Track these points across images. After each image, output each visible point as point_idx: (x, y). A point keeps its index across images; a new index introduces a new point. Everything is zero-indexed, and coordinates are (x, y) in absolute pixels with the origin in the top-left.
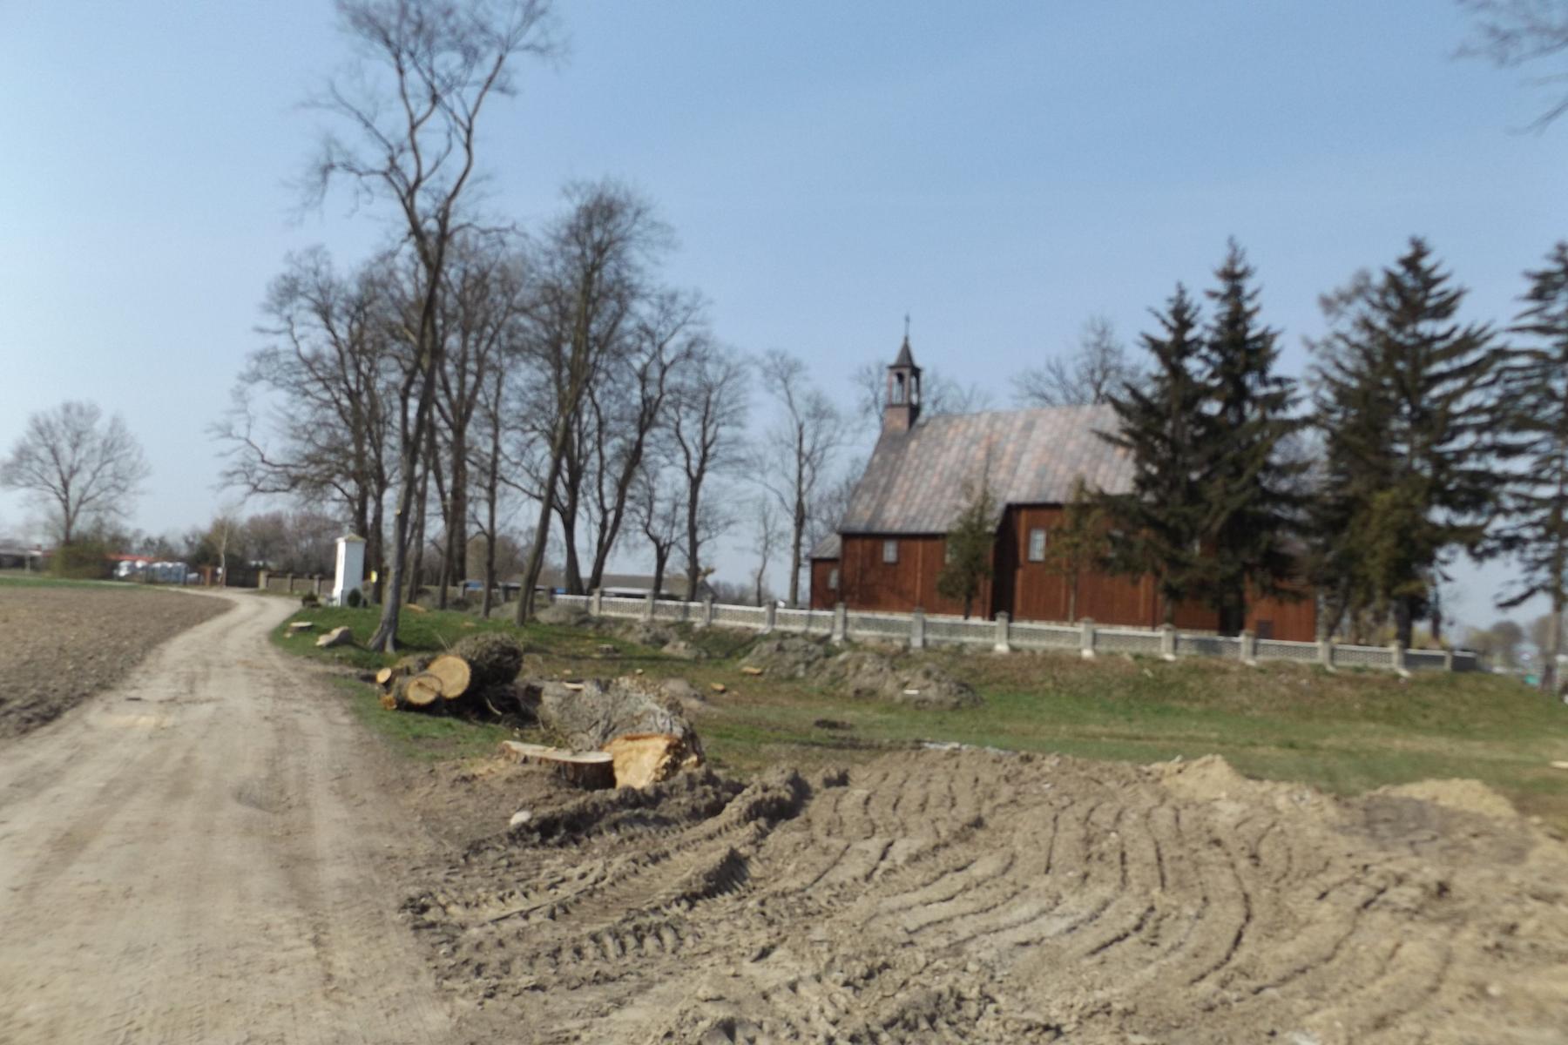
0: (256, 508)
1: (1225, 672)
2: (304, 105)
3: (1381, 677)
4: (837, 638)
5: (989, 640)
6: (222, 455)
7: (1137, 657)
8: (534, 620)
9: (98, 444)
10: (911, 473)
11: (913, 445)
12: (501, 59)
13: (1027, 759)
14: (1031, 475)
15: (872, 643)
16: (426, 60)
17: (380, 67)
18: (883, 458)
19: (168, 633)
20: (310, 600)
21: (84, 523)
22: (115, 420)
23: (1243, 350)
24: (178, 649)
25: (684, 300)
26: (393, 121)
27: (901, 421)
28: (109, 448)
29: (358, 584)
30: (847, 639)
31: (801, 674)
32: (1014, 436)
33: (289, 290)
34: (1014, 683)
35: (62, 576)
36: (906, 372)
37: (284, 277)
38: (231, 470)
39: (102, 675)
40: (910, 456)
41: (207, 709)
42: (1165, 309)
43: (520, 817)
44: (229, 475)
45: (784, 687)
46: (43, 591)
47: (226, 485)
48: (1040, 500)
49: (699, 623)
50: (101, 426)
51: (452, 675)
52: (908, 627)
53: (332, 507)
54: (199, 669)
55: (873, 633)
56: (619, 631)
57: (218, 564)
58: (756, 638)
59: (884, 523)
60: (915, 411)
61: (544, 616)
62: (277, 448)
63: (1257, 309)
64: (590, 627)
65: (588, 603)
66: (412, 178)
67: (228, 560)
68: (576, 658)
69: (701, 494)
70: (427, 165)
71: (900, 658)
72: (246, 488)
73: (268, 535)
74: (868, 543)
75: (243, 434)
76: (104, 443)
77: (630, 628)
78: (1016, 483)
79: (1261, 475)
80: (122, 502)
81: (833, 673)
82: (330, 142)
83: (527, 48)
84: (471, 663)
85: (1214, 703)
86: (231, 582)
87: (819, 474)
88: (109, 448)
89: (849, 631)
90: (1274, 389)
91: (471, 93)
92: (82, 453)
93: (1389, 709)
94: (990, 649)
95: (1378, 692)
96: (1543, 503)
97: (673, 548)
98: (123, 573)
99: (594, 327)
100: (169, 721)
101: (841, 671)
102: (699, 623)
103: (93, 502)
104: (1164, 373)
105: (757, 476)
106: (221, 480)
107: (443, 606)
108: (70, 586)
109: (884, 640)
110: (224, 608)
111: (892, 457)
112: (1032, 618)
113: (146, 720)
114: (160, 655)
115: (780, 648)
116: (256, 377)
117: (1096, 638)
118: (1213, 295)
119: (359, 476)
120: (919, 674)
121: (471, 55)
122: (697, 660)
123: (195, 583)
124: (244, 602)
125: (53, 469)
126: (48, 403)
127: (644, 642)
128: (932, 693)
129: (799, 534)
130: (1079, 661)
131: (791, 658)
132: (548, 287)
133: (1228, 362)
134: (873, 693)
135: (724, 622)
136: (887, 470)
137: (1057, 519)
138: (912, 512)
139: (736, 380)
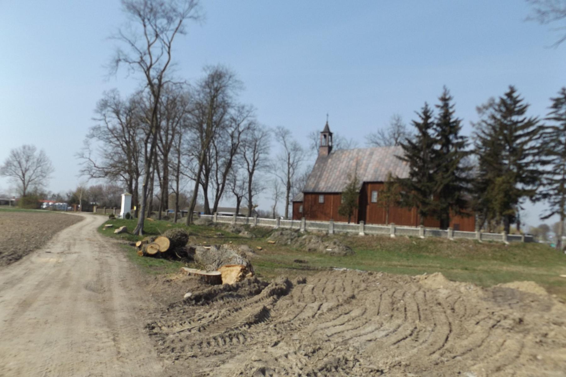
0: (92, 183)
1: (442, 242)
2: (110, 38)
3: (499, 244)
4: (302, 230)
5: (357, 231)
6: (80, 164)
7: (410, 237)
8: (193, 224)
9: (35, 160)
10: (329, 171)
11: (330, 160)
12: (181, 21)
14: (372, 172)
15: (315, 232)
16: (154, 22)
17: (137, 24)
18: (319, 165)
19: (60, 228)
20: (112, 216)
21: (30, 189)
22: (41, 152)
23: (449, 126)
24: (64, 234)
25: (247, 108)
26: (142, 44)
27: (325, 152)
28: (39, 162)
29: (129, 211)
30: (306, 230)
31: (289, 243)
32: (366, 157)
33: (104, 105)
34: (366, 246)
35: (23, 208)
36: (327, 134)
37: (103, 100)
38: (83, 169)
39: (37, 243)
40: (328, 164)
41: (75, 256)
42: (420, 111)
43: (188, 295)
44: (83, 171)
45: (283, 248)
46: (15, 213)
47: (81, 175)
48: (375, 180)
49: (252, 225)
50: (36, 154)
51: (163, 243)
52: (328, 226)
53: (120, 183)
54: (72, 241)
55: (315, 228)
56: (224, 228)
57: (79, 204)
58: (273, 230)
59: (319, 189)
60: (330, 148)
61: (196, 222)
62: (100, 161)
63: (454, 112)
64: (213, 226)
65: (212, 218)
66: (149, 64)
67: (82, 202)
68: (208, 237)
69: (253, 178)
70: (154, 59)
71: (325, 237)
72: (89, 176)
74: (313, 196)
75: (88, 156)
76: (38, 160)
77: (227, 227)
78: (367, 174)
79: (455, 171)
80: (44, 181)
81: (301, 243)
82: (119, 51)
83: (190, 17)
84: (170, 239)
85: (438, 254)
86: (83, 210)
87: (296, 171)
88: (39, 162)
89: (307, 228)
90: (460, 140)
91: (170, 34)
92: (30, 163)
93: (501, 256)
94: (357, 234)
95: (497, 250)
96: (557, 181)
97: (243, 198)
98: (44, 207)
100: (61, 260)
101: (304, 242)
102: (252, 225)
104: (420, 134)
105: (273, 172)
106: (80, 173)
107: (160, 219)
108: (25, 211)
109: (319, 231)
110: (81, 219)
111: (322, 165)
112: (372, 223)
113: (53, 260)
114: (58, 236)
115: (282, 234)
116: (92, 136)
117: (395, 230)
118: (438, 106)
119: (130, 172)
120: (332, 243)
121: (170, 20)
122: (252, 238)
123: (71, 210)
124: (88, 217)
125: (19, 169)
126: (17, 145)
127: (232, 232)
128: (336, 250)
129: (288, 193)
130: (390, 238)
131: (286, 237)
132: (198, 103)
133: (443, 130)
134: (315, 250)
135: (261, 225)
136: (320, 169)
137: (381, 187)
138: (329, 185)
139: (266, 137)
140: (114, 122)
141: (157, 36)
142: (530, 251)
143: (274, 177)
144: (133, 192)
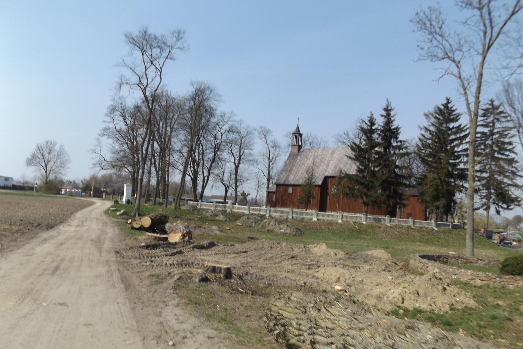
0: (101, 173)
1: (380, 227)
2: (116, 66)
3: (428, 230)
4: (267, 215)
5: (312, 217)
6: (93, 158)
7: (354, 222)
8: (180, 209)
10: (298, 166)
11: (299, 157)
12: (170, 52)
13: (279, 243)
14: (333, 168)
15: (277, 217)
16: (149, 52)
17: (138, 53)
18: (290, 162)
19: (77, 210)
20: (116, 202)
21: (51, 177)
22: (61, 146)
23: (390, 133)
24: (79, 214)
25: (227, 115)
26: (140, 70)
27: (296, 151)
28: (59, 155)
29: (130, 198)
30: (270, 216)
31: (253, 225)
32: (328, 155)
33: (113, 109)
34: (317, 229)
35: (45, 193)
36: (297, 135)
37: (112, 105)
38: (95, 163)
39: (62, 219)
40: (298, 161)
41: (86, 227)
42: (367, 120)
43: (143, 244)
44: (95, 164)
45: (248, 229)
46: (42, 198)
47: (94, 167)
49: (228, 210)
50: (57, 148)
51: (147, 222)
52: (288, 213)
53: (125, 172)
54: (84, 219)
55: (278, 214)
56: (204, 212)
57: (91, 190)
58: (244, 215)
59: (289, 181)
60: (300, 147)
61: (183, 208)
62: (109, 156)
63: (394, 120)
64: (196, 211)
65: (197, 204)
66: (145, 85)
67: (93, 189)
68: (190, 220)
69: (239, 171)
70: (149, 81)
71: (280, 222)
72: (100, 168)
73: (107, 181)
74: (284, 187)
75: (99, 152)
76: (58, 153)
77: (207, 212)
78: (328, 170)
80: (63, 171)
81: (262, 225)
82: (122, 77)
83: (177, 48)
84: (151, 219)
85: (375, 236)
86: (95, 196)
87: (275, 165)
88: (59, 155)
89: (271, 213)
90: (399, 144)
91: (161, 61)
92: (51, 156)
94: (311, 219)
95: (425, 234)
96: (485, 178)
97: (230, 187)
98: (63, 193)
100: (78, 229)
101: (264, 225)
102: (228, 210)
103: (54, 171)
104: (366, 138)
105: (256, 165)
106: (93, 166)
107: (155, 204)
108: (48, 197)
109: (281, 216)
110: (92, 204)
111: (293, 161)
113: (72, 229)
114: (75, 216)
115: (248, 218)
116: (104, 135)
118: (382, 116)
119: (133, 166)
120: (285, 226)
121: (162, 50)
122: (226, 221)
123: (84, 196)
124: (98, 202)
125: (43, 161)
126: (41, 141)
127: (211, 216)
128: (288, 231)
129: (268, 184)
130: (337, 223)
131: (251, 221)
133: (385, 135)
134: (272, 231)
135: (235, 210)
136: (291, 165)
138: (297, 178)
139: (250, 135)
140: (121, 125)
141: (152, 63)
142: (453, 236)
143: (256, 170)
144: (135, 182)
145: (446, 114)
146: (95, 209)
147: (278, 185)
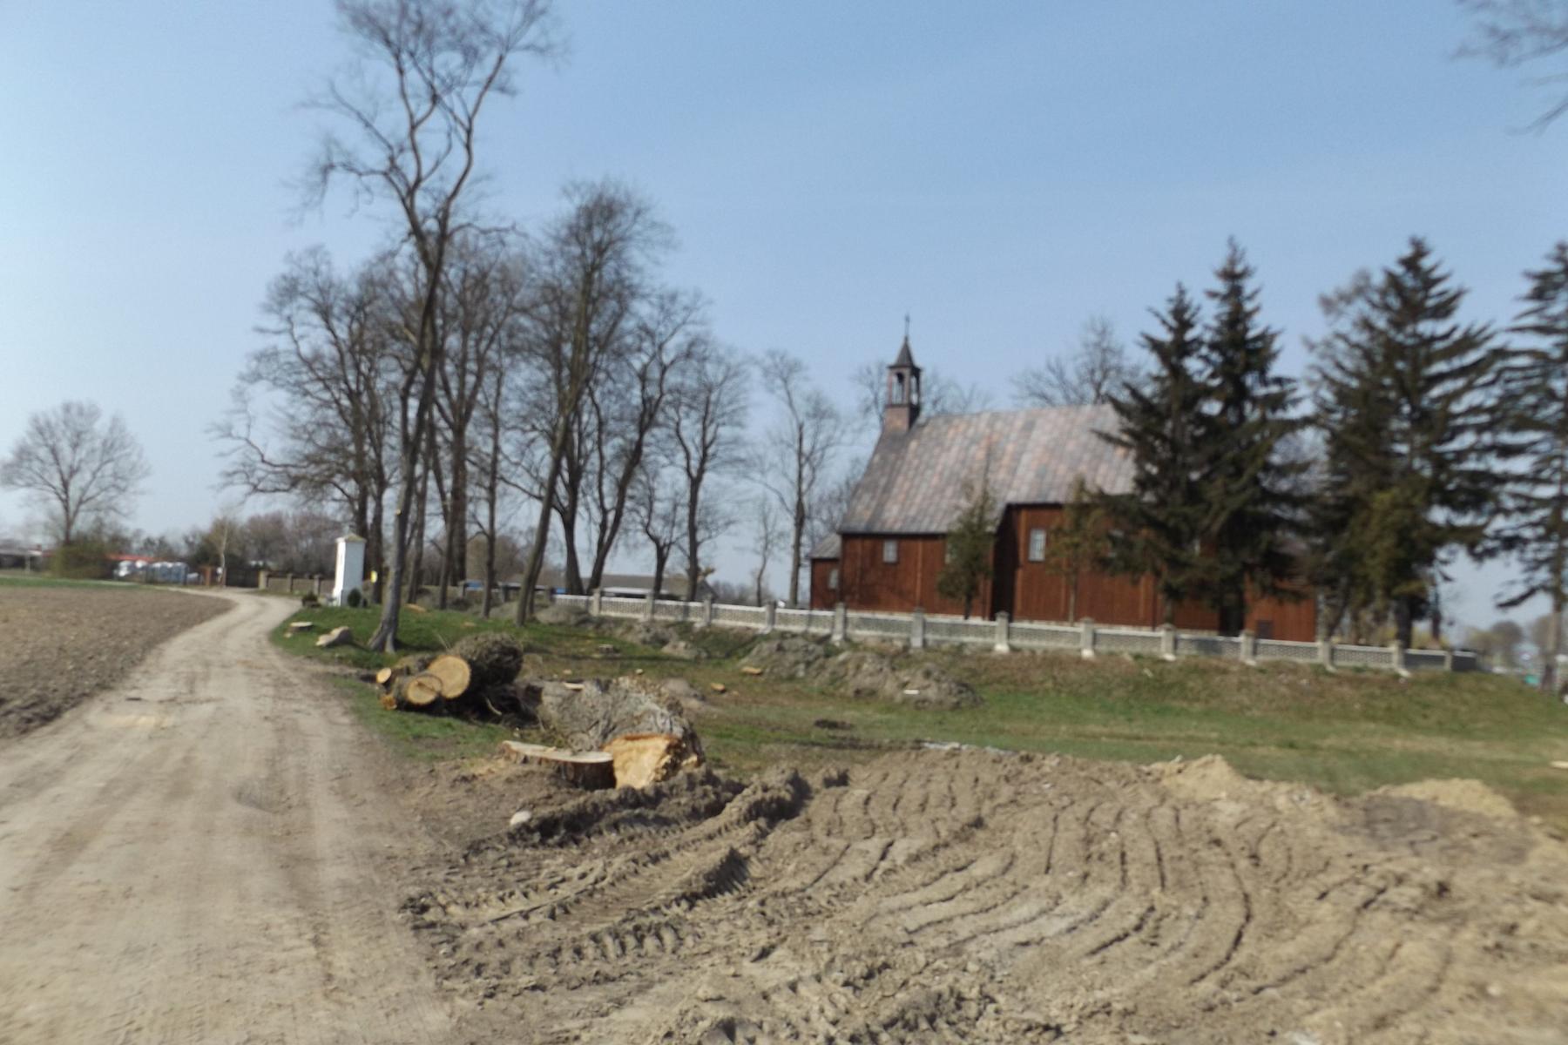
0: (256, 508)
1: (1225, 672)
2: (304, 105)
3: (1381, 677)
4: (837, 638)
5: (989, 640)
6: (222, 455)
7: (1137, 657)
8: (534, 620)
9: (98, 444)
10: (911, 473)
11: (913, 445)
12: (501, 59)
14: (1031, 475)
15: (872, 643)
16: (426, 60)
17: (380, 67)
18: (883, 458)
19: (168, 633)
20: (310, 600)
21: (84, 523)
22: (115, 420)
23: (1243, 350)
24: (178, 649)
25: (684, 300)
26: (393, 121)
27: (901, 421)
28: (109, 448)
29: (358, 584)
30: (847, 639)
31: (801, 674)
32: (1014, 436)
33: (289, 290)
34: (1014, 683)
35: (62, 576)
36: (906, 372)
37: (284, 277)
38: (231, 470)
39: (102, 675)
40: (910, 456)
42: (1165, 309)
43: (520, 817)
44: (229, 475)
45: (784, 687)
46: (43, 591)
47: (226, 485)
48: (1040, 500)
49: (699, 623)
50: (101, 426)
51: (452, 675)
52: (908, 627)
53: (332, 507)
54: (199, 669)
55: (873, 633)
56: (619, 631)
57: (218, 564)
58: (756, 638)
59: (884, 523)
60: (915, 411)
61: (544, 616)
62: (277, 448)
63: (1257, 309)
64: (590, 627)
65: (588, 603)
66: (412, 178)
67: (228, 560)
68: (576, 658)
69: (701, 494)
70: (427, 165)
71: (900, 658)
72: (246, 488)
73: (268, 535)
74: (868, 543)
75: (243, 434)
76: (104, 443)
77: (630, 628)
78: (1016, 483)
79: (1261, 475)
80: (122, 502)
81: (833, 673)
82: (330, 142)
83: (527, 48)
84: (471, 663)
85: (1214, 703)
86: (231, 582)
87: (819, 474)
88: (109, 448)
89: (849, 631)
90: (1274, 389)
91: (471, 93)
92: (82, 453)
93: (1389, 709)
94: (990, 649)
95: (1378, 692)
96: (1543, 503)
97: (673, 548)
98: (123, 573)
99: (594, 327)
100: (169, 721)
101: (841, 671)
102: (699, 623)
104: (1164, 373)
105: (757, 476)
106: (221, 480)
107: (443, 606)
108: (70, 586)
109: (884, 640)
110: (224, 608)
111: (892, 457)
112: (1032, 618)
113: (146, 720)
114: (160, 655)
115: (780, 648)
116: (256, 377)
117: (1096, 638)
118: (1213, 295)
119: (359, 476)
120: (919, 674)
121: (471, 55)
122: (697, 660)
123: (195, 583)
124: (244, 602)
125: (53, 469)
126: (48, 403)
127: (644, 642)
128: (932, 693)
129: (799, 534)
130: (1079, 661)
131: (791, 658)
132: (548, 287)
133: (1228, 362)
134: (873, 693)
135: (724, 622)
136: (887, 470)
137: (1057, 519)
138: (912, 512)
139: (736, 380)
140: (315, 338)
142: (1468, 696)
145: (1413, 290)
146: (235, 626)
147: (848, 536)
